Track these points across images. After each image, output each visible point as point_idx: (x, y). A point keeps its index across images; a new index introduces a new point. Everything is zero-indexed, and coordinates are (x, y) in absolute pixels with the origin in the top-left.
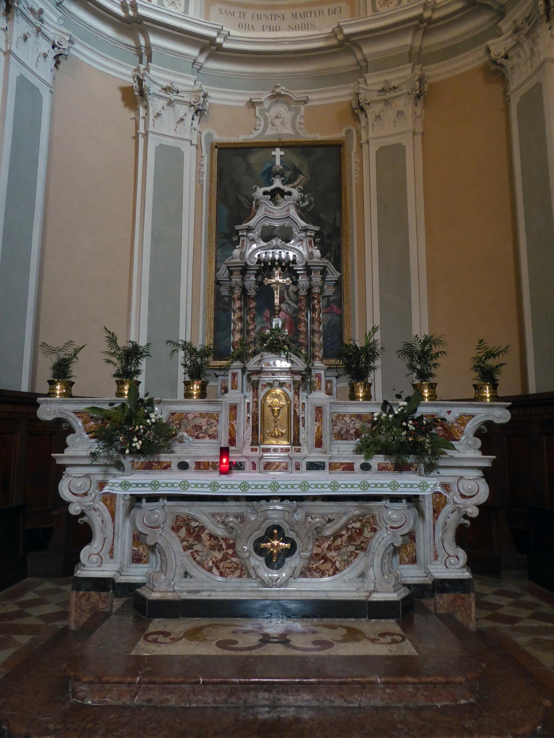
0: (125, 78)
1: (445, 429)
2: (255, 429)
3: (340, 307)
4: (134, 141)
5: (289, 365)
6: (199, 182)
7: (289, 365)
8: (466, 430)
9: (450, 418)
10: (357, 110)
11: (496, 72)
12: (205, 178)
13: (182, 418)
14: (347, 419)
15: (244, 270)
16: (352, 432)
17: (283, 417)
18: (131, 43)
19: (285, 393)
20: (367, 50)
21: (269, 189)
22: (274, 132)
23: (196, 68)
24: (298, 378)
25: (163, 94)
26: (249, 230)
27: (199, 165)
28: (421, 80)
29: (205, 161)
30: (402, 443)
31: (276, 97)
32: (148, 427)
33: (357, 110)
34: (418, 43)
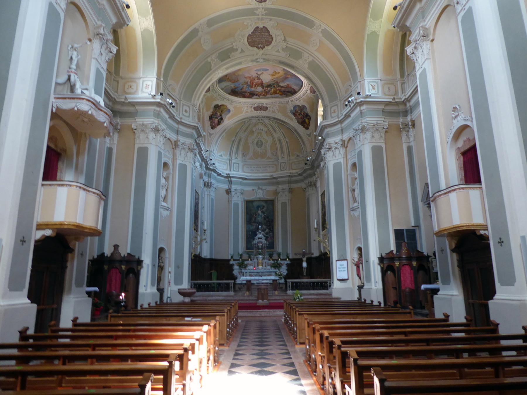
10: (276, 193)
31: (259, 188)
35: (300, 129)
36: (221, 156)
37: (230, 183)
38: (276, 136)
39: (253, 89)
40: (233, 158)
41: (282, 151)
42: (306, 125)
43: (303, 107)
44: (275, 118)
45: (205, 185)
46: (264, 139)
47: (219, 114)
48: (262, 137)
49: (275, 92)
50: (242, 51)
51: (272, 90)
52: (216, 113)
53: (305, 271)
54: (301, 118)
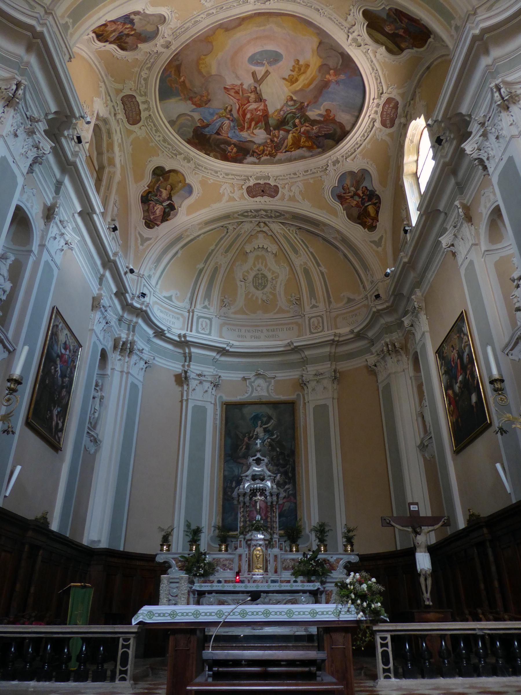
0: (177, 370)
1: (330, 565)
2: (249, 565)
3: (295, 498)
4: (180, 403)
5: (263, 537)
6: (215, 424)
7: (263, 537)
8: (339, 566)
9: (332, 560)
11: (372, 371)
12: (218, 422)
13: (218, 560)
14: (288, 561)
15: (245, 494)
16: (291, 567)
17: (261, 560)
18: (181, 351)
19: (262, 549)
20: (307, 353)
21: (255, 458)
22: (257, 394)
23: (215, 361)
24: (267, 542)
25: (197, 378)
26: (247, 476)
27: (215, 414)
28: (335, 371)
29: (218, 412)
30: (309, 570)
32: (205, 565)
33: (302, 384)
34: (333, 350)
35: (356, 233)
36: (170, 298)
37: (188, 358)
38: (298, 261)
39: (245, 135)
40: (198, 306)
42: (369, 221)
43: (364, 173)
44: (296, 217)
45: (115, 347)
46: (270, 270)
47: (165, 194)
48: (266, 266)
49: (296, 145)
51: (290, 136)
52: (158, 190)
53: (426, 587)
54: (357, 205)
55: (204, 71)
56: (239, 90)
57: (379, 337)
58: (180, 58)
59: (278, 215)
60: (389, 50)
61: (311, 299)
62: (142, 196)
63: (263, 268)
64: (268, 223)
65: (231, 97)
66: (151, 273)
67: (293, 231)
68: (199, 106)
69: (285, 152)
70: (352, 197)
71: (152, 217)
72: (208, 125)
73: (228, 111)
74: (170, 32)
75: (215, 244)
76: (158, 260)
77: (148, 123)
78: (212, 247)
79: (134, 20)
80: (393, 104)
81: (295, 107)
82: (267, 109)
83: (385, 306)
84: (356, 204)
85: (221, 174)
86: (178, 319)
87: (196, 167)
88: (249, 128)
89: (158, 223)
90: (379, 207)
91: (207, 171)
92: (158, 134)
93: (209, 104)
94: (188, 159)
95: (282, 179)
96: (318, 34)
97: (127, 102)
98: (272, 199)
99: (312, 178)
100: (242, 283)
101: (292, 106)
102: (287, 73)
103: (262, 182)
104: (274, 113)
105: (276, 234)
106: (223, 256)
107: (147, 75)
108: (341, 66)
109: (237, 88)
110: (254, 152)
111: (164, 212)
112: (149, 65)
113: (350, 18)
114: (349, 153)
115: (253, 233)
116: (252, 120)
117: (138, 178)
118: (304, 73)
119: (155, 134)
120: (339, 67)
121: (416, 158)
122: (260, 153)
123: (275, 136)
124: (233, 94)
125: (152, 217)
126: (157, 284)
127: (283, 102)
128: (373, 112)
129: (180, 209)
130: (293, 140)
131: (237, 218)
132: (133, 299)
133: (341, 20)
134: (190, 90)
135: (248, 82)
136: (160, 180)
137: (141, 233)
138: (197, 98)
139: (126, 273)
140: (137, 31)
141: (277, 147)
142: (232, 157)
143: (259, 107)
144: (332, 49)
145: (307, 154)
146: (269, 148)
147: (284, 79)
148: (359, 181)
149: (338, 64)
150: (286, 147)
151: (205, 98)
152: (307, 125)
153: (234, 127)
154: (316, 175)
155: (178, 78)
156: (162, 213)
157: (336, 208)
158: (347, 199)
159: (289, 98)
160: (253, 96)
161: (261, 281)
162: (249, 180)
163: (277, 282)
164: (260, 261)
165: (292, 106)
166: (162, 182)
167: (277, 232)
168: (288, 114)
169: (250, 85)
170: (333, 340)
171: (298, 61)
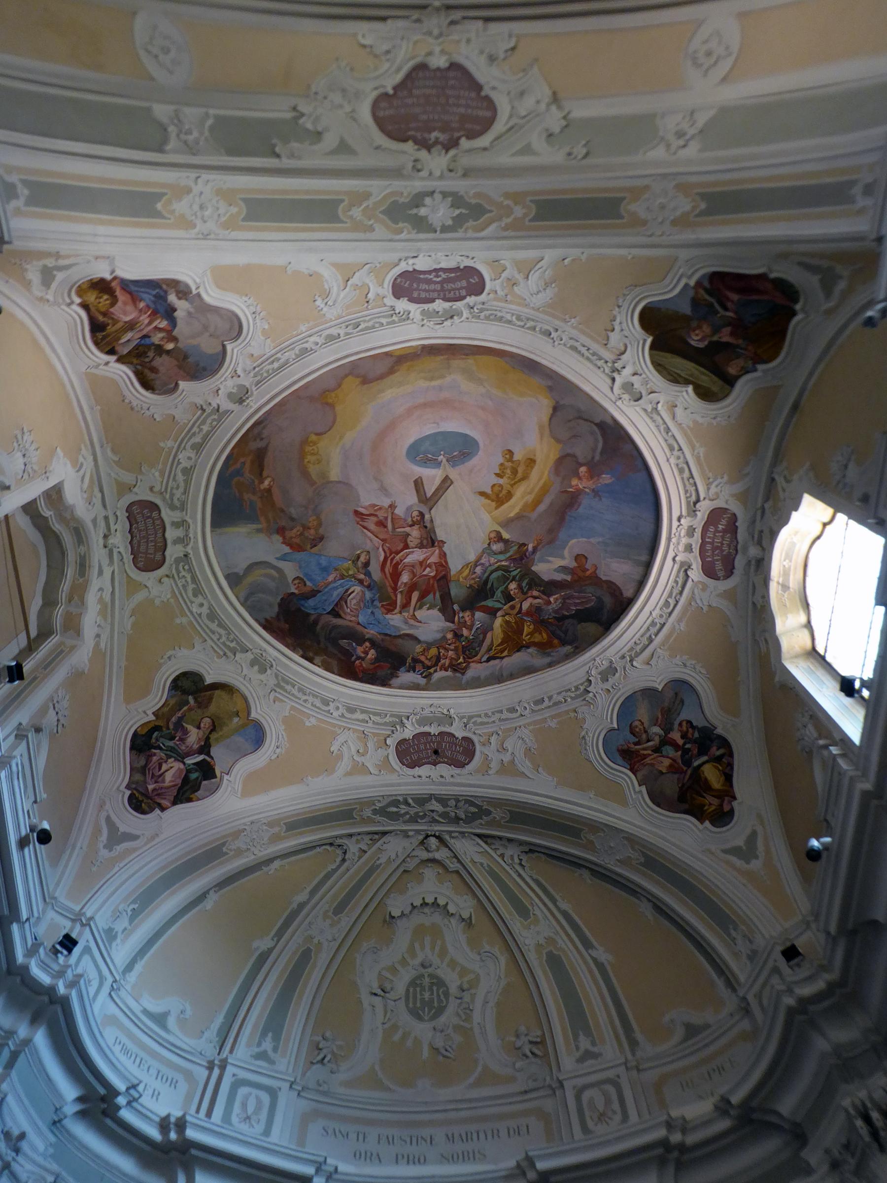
35: (682, 837)
36: (160, 1019)
38: (530, 937)
39: (396, 621)
41: (579, 1020)
42: (711, 802)
43: (680, 689)
46: (453, 964)
47: (194, 737)
48: (443, 953)
49: (514, 641)
50: (343, 148)
51: (498, 622)
52: (179, 725)
54: (673, 769)
55: (313, 470)
56: (386, 518)
57: (822, 1100)
58: (265, 433)
59: (473, 812)
60: (704, 394)
61: (576, 1037)
62: (135, 734)
63: (436, 961)
64: (447, 837)
65: (369, 534)
66: (119, 927)
67: (512, 857)
68: (297, 548)
69: (488, 660)
70: (657, 750)
71: (150, 787)
72: (314, 593)
73: (359, 563)
74: (249, 365)
75: (309, 889)
76: (146, 898)
77: (178, 572)
78: (302, 897)
79: (175, 310)
80: (724, 522)
81: (508, 555)
82: (446, 562)
83: (820, 985)
84: (671, 766)
85: (338, 708)
86: (174, 1083)
87: (278, 685)
88: (406, 605)
89: (165, 803)
90: (731, 765)
91: (305, 698)
92: (200, 599)
93: (320, 546)
94: (261, 664)
95: (482, 724)
96: (550, 389)
97: (139, 518)
98: (458, 771)
99: (553, 717)
100: (377, 1001)
101: (501, 553)
102: (488, 481)
103: (434, 730)
104: (461, 572)
105: (470, 866)
106: (328, 921)
107: (191, 463)
108: (601, 453)
109: (381, 515)
110: (416, 661)
111: (186, 780)
112: (197, 439)
113: (614, 337)
114: (638, 648)
115: (411, 865)
116: (412, 587)
117: (135, 690)
118: (524, 479)
119: (193, 599)
120: (597, 458)
121: (803, 619)
122: (429, 664)
123: (464, 624)
124: (372, 527)
125: (150, 787)
126: (129, 967)
127: (480, 546)
128: (681, 548)
129: (226, 777)
130: (504, 632)
131: (369, 821)
132: (31, 952)
133: (595, 347)
134: (282, 511)
135: (406, 501)
136: (187, 703)
137: (114, 817)
138: (295, 531)
139: (23, 843)
140: (179, 345)
141: (469, 650)
142: (364, 671)
143: (427, 558)
144: (580, 418)
145: (539, 661)
146: (450, 653)
147: (482, 494)
148: (669, 710)
149: (594, 450)
150: (490, 649)
151: (312, 531)
152: (535, 593)
153: (373, 601)
154: (564, 708)
155: (257, 480)
156: (179, 781)
157: (620, 780)
158: (645, 757)
159: (493, 535)
160: (415, 533)
161: (428, 996)
162: (403, 725)
163: (473, 996)
164: (428, 940)
165: (501, 553)
166: (190, 709)
167: (472, 861)
168: (492, 572)
169: (409, 509)
170: (664, 1143)
171: (511, 453)
